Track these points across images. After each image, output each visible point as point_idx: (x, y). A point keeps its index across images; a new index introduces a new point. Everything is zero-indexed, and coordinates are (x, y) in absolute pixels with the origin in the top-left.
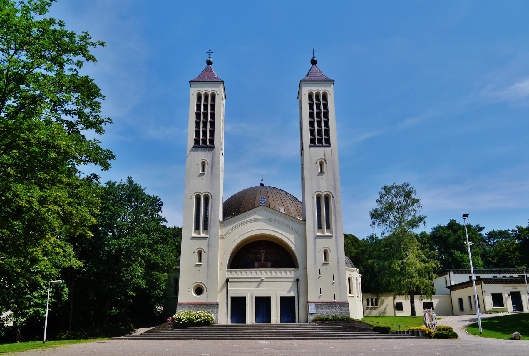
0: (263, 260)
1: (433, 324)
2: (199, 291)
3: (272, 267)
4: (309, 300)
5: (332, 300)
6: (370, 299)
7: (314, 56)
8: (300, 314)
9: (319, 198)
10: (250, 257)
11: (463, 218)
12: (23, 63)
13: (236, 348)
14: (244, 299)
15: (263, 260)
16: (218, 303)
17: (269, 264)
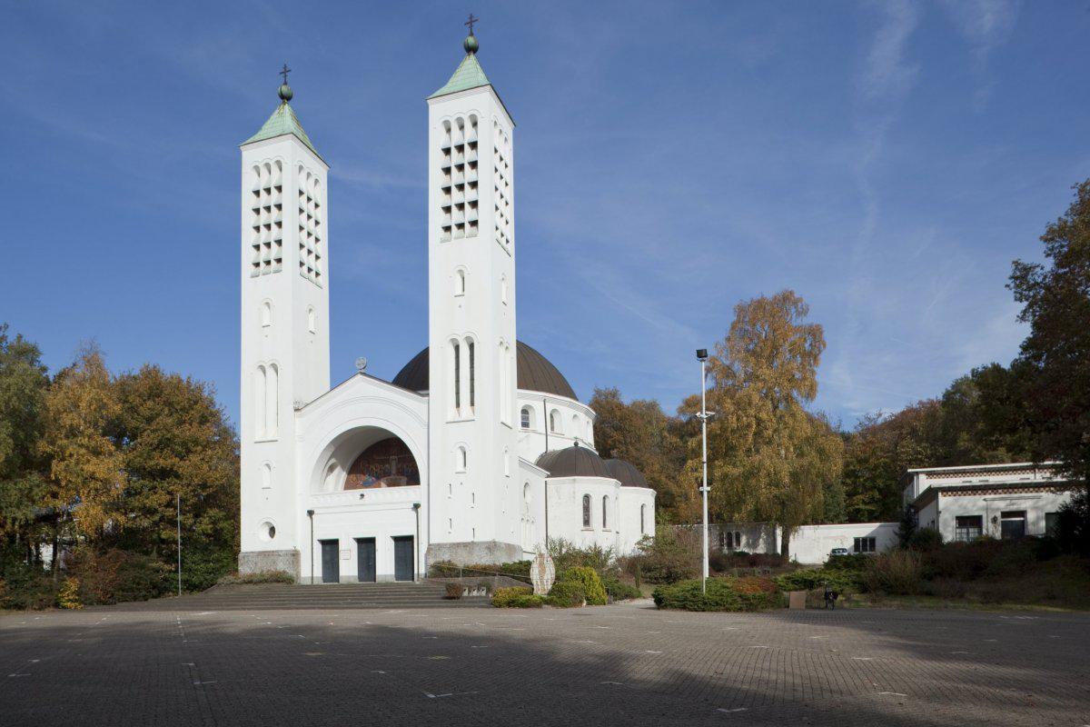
0: (394, 472)
2: (272, 531)
5: (469, 539)
8: (421, 568)
14: (371, 541)
17: (405, 479)
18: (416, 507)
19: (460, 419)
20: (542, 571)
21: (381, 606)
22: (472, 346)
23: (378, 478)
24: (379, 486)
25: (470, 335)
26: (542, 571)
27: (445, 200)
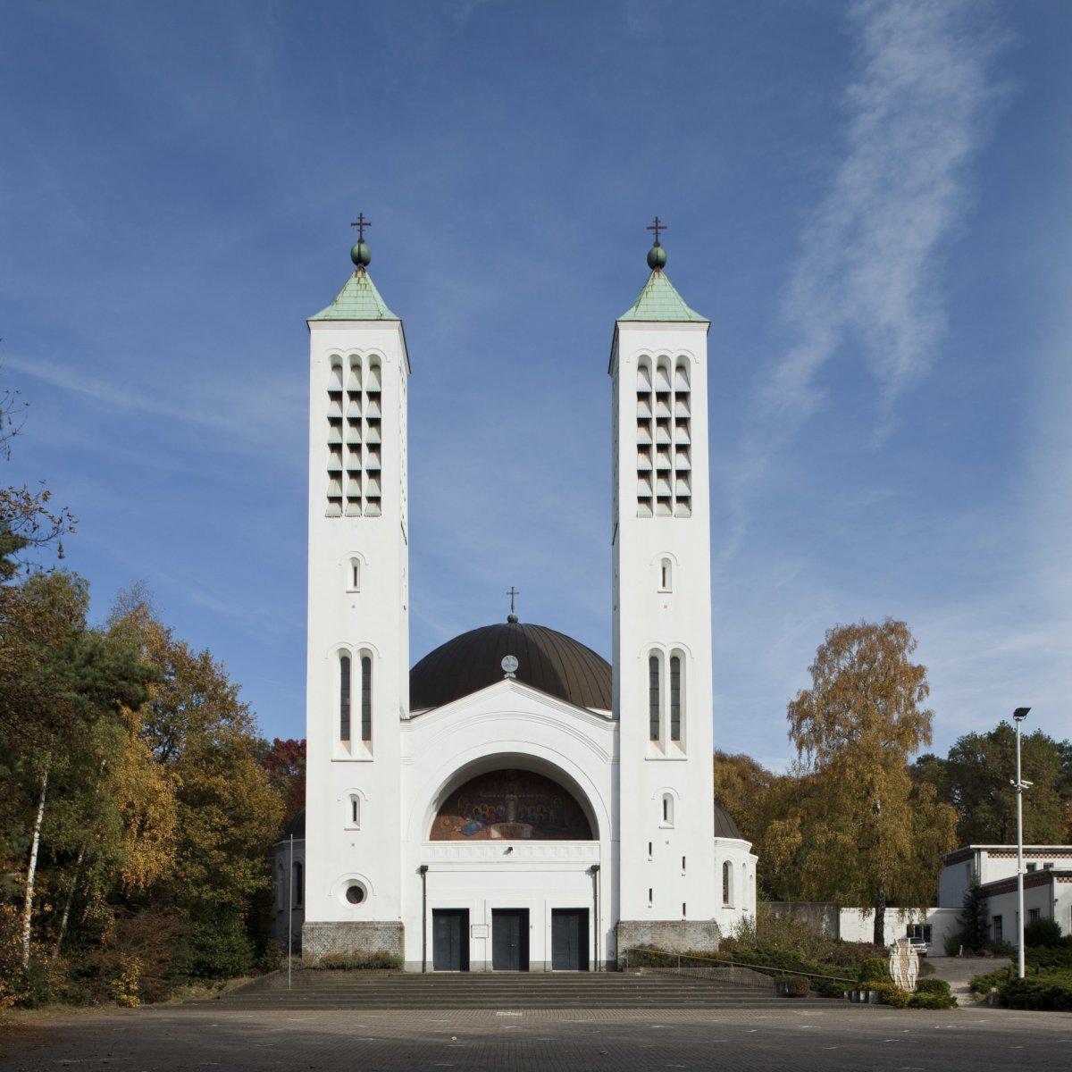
2: (356, 894)
3: (535, 836)
4: (622, 919)
5: (678, 917)
7: (659, 240)
8: (599, 950)
9: (654, 662)
10: (480, 810)
11: (1016, 718)
12: (131, 814)
13: (439, 1026)
14: (463, 914)
16: (400, 923)
17: (528, 829)
18: (595, 869)
19: (349, 758)
20: (906, 963)
21: (739, 1005)
23: (487, 822)
24: (488, 837)
25: (366, 646)
27: (642, 462)
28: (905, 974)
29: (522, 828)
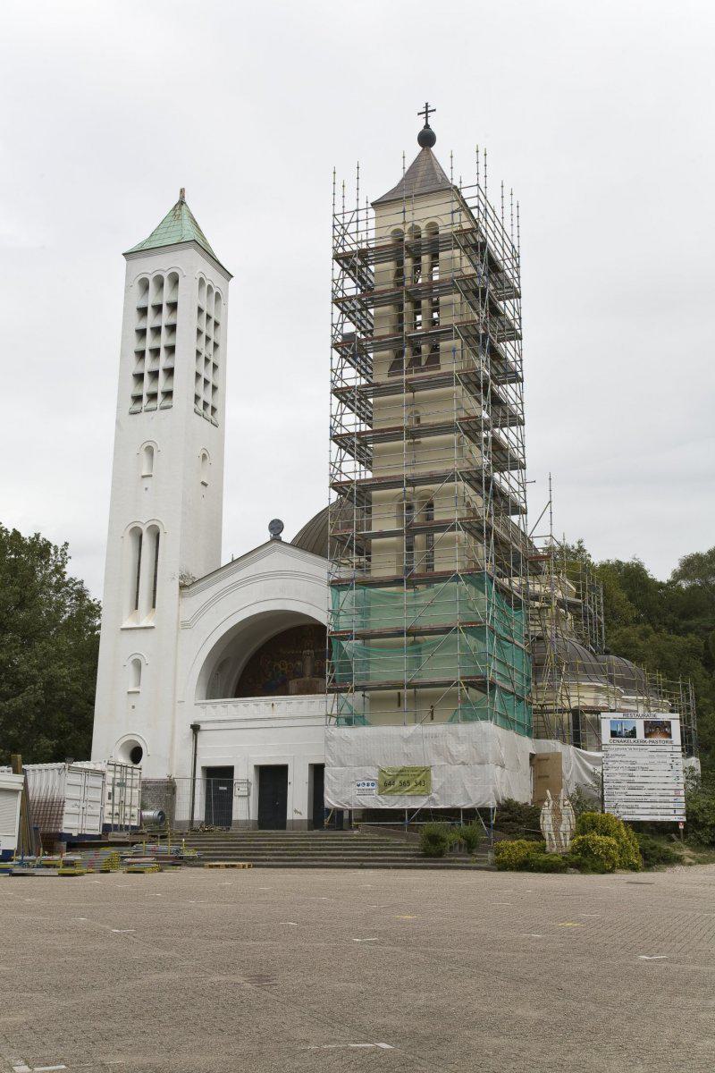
0: (308, 672)
1: (562, 834)
6: (245, 776)
10: (280, 666)
14: (282, 770)
15: (308, 672)
20: (558, 819)
22: (157, 537)
26: (558, 819)
28: (557, 831)
29: (318, 682)
